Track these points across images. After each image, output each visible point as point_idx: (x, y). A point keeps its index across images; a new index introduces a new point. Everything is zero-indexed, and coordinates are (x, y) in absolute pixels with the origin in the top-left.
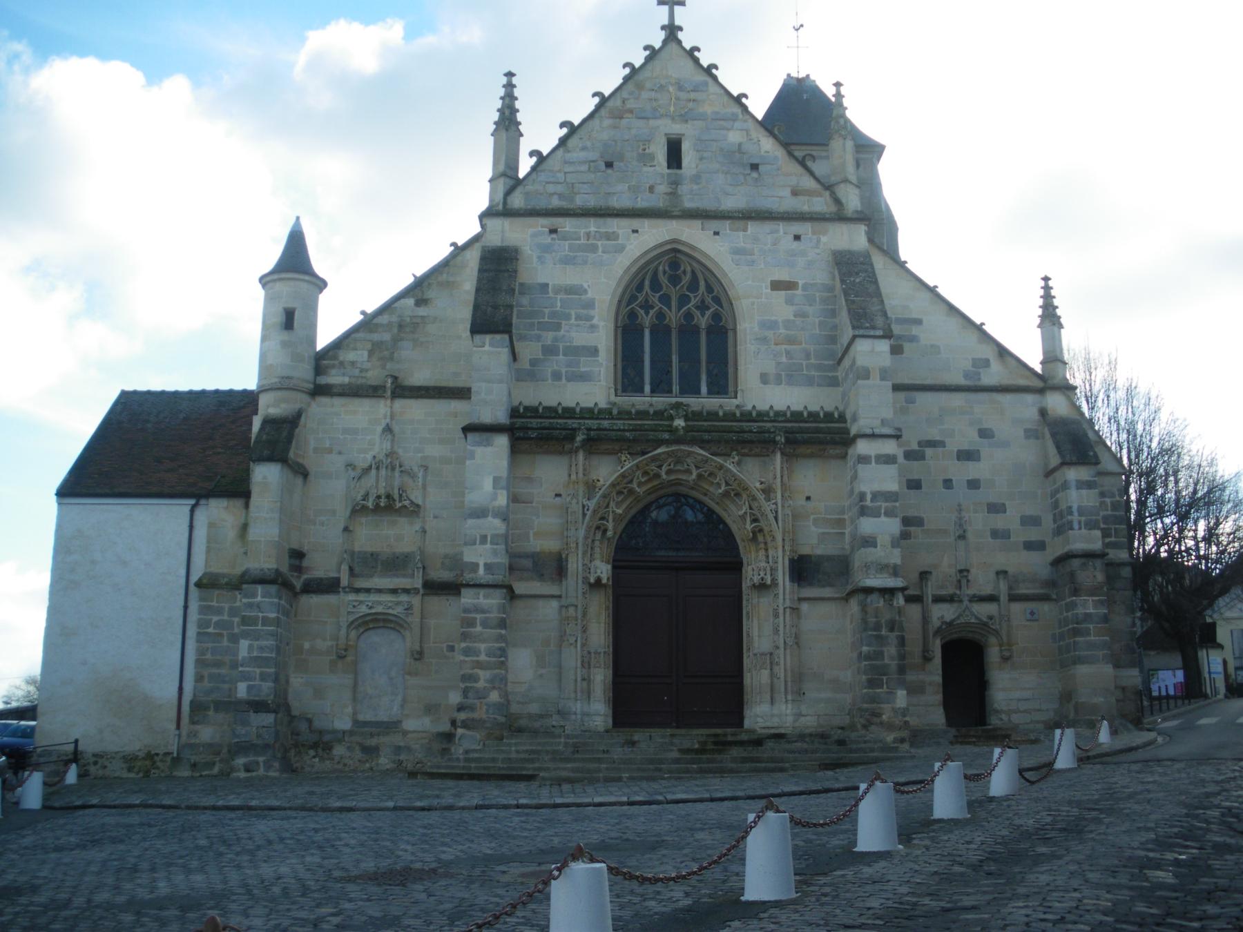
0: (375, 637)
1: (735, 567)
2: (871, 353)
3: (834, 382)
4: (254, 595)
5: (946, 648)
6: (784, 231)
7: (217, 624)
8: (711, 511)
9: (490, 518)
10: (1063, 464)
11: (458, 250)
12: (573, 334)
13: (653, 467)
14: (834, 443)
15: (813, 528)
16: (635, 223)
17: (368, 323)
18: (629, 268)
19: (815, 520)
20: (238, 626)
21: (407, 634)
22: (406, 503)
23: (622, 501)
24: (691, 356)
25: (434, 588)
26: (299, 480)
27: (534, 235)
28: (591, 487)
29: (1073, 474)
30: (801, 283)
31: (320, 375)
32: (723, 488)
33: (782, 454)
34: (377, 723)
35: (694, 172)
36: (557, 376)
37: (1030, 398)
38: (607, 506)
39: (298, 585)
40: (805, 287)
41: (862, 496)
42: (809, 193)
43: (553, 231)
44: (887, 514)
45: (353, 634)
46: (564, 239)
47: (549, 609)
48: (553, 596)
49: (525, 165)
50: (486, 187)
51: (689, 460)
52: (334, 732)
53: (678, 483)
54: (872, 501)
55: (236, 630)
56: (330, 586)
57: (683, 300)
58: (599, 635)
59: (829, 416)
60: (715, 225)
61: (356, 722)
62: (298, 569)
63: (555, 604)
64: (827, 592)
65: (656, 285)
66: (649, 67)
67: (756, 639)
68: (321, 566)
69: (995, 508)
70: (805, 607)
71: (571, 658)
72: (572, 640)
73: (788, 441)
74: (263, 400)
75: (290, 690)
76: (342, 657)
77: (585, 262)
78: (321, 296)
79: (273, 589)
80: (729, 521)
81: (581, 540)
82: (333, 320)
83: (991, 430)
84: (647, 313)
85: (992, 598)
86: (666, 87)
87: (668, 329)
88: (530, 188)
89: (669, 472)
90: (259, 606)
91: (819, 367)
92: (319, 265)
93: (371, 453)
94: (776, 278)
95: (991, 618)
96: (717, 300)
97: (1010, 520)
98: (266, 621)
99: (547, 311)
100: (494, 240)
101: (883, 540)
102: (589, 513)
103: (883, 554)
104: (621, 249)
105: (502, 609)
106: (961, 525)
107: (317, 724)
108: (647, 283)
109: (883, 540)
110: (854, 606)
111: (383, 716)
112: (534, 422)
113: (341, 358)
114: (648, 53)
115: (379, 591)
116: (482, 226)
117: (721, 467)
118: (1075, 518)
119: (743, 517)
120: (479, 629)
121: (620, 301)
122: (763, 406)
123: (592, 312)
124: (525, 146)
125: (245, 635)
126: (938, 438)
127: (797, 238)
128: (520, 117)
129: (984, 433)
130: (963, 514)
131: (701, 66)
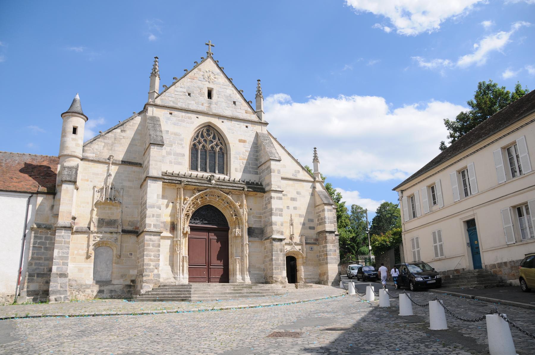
3: (257, 173)
4: (61, 233)
6: (243, 125)
7: (39, 243)
24: (204, 160)
36: (171, 162)
43: (171, 114)
52: (86, 285)
55: (48, 246)
59: (257, 184)
65: (202, 136)
91: (253, 168)
102: (185, 209)
104: (193, 123)
107: (79, 282)
120: (151, 247)
129: (298, 193)
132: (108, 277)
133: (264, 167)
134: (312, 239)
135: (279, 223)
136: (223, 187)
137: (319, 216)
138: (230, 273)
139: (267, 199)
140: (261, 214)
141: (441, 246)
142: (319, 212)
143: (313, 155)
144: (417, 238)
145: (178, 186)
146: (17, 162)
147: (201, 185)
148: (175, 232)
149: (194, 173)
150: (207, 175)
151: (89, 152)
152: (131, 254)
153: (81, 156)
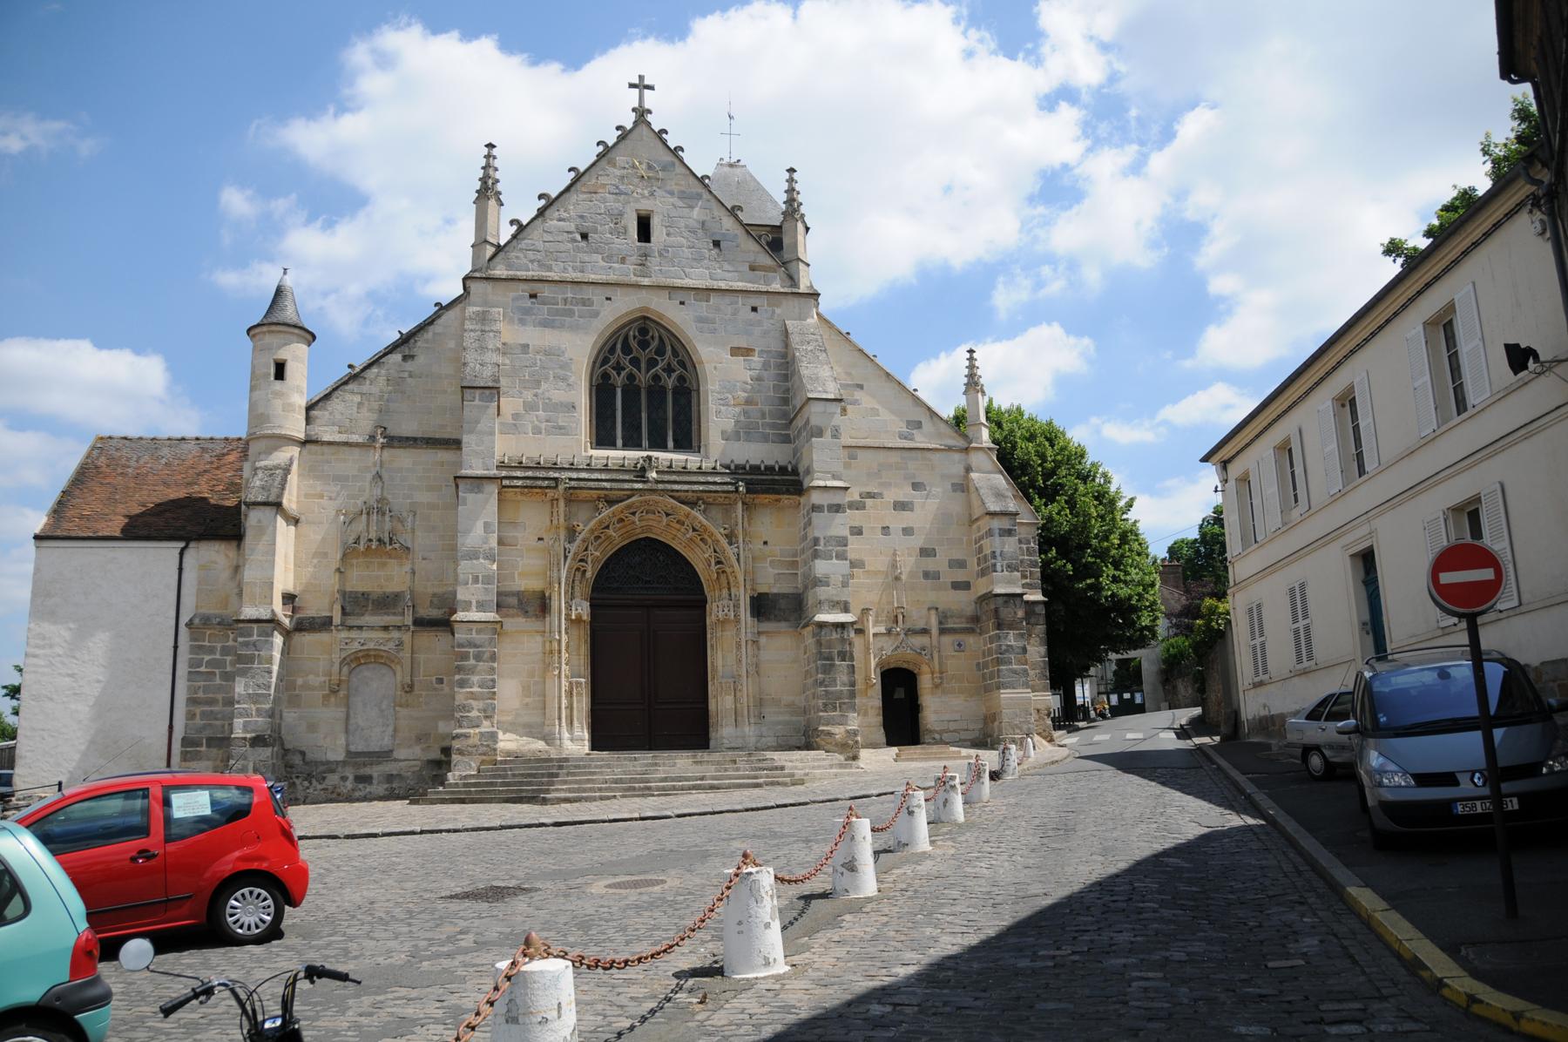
3: (786, 440)
7: (209, 663)
36: (537, 431)
43: (533, 296)
52: (328, 762)
55: (229, 669)
59: (783, 470)
65: (627, 349)
85: (925, 631)
91: (773, 426)
107: (309, 756)
120: (472, 662)
133: (799, 422)
134: (960, 617)
135: (836, 579)
136: (676, 487)
140: (795, 555)
141: (1307, 629)
142: (981, 538)
143: (966, 372)
144: (1259, 606)
145: (551, 493)
146: (163, 461)
147: (615, 485)
150: (634, 455)
152: (440, 681)
153: (302, 436)
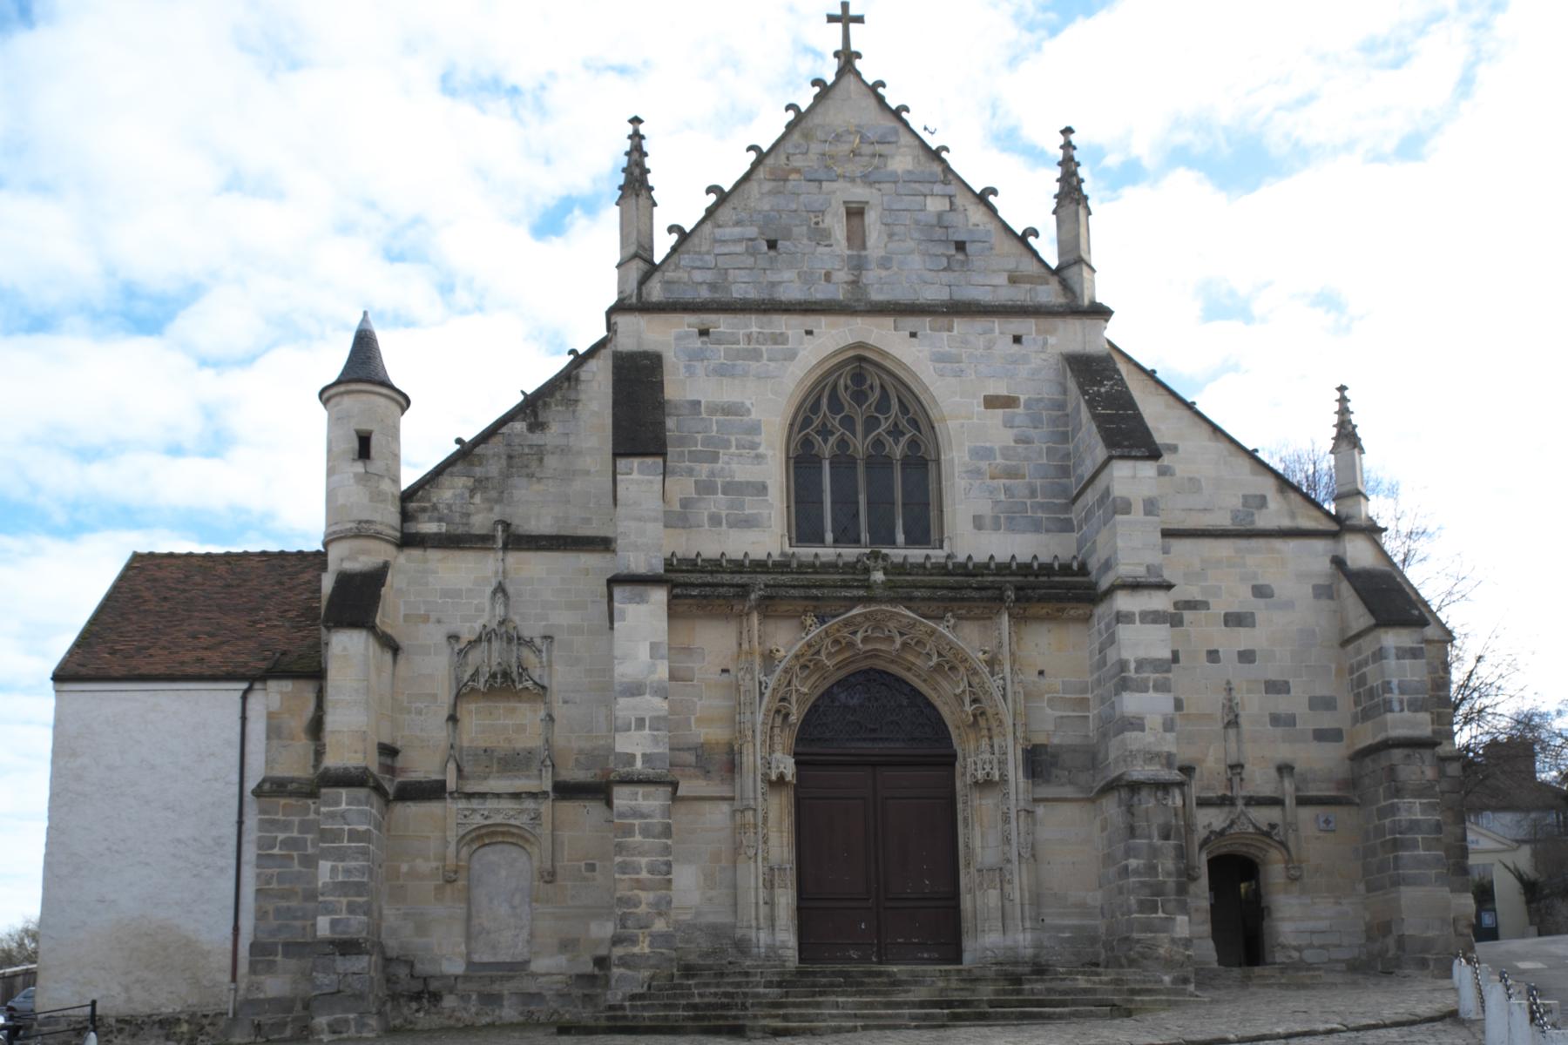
0: (492, 855)
1: (948, 760)
2: (1130, 478)
3: (1066, 527)
4: (338, 803)
5: (1214, 863)
6: (1001, 329)
7: (284, 843)
8: (915, 692)
9: (647, 697)
10: (1377, 625)
11: (579, 360)
12: (734, 466)
13: (845, 632)
14: (1078, 599)
15: (1048, 711)
16: (810, 321)
17: (466, 453)
18: (802, 381)
19: (1050, 700)
20: (314, 845)
21: (535, 851)
22: (529, 684)
23: (807, 678)
24: (845, 502)
25: (566, 791)
26: (388, 657)
27: (679, 338)
28: (769, 658)
29: (1392, 639)
30: (1022, 398)
31: (418, 519)
32: (935, 659)
33: (1010, 615)
34: (498, 964)
35: (882, 253)
36: (715, 520)
37: (1320, 545)
38: (789, 684)
39: (390, 789)
40: (1028, 405)
41: (1123, 665)
42: (1030, 279)
43: (704, 333)
44: (1157, 688)
45: (465, 852)
46: (719, 342)
47: (718, 815)
48: (723, 799)
49: (662, 245)
50: (614, 275)
51: (891, 625)
52: (443, 977)
53: (875, 654)
54: (1137, 670)
55: (310, 851)
56: (432, 791)
57: (872, 423)
58: (780, 846)
59: (1066, 569)
60: (911, 323)
61: (470, 964)
62: (391, 770)
63: (725, 807)
64: (1068, 792)
66: (819, 110)
67: (978, 850)
68: (422, 766)
69: (1276, 687)
70: (1040, 810)
71: (751, 876)
72: (751, 852)
73: (1018, 600)
74: (334, 554)
75: (384, 925)
76: (450, 881)
77: (745, 374)
78: (403, 419)
79: (362, 793)
80: (938, 703)
81: (759, 728)
82: (421, 447)
83: (1268, 586)
84: (826, 441)
85: (1276, 802)
86: (845, 137)
87: (852, 461)
88: (670, 275)
89: (865, 640)
90: (343, 815)
92: (397, 375)
93: (481, 622)
94: (991, 392)
95: (1273, 826)
96: (914, 423)
97: (1294, 704)
98: (354, 836)
99: (699, 437)
100: (625, 343)
101: (1154, 721)
102: (768, 693)
103: (1152, 739)
105: (668, 812)
106: (1231, 708)
108: (825, 401)
109: (1154, 721)
110: (1111, 807)
111: (504, 957)
112: (694, 578)
113: (434, 500)
114: (817, 90)
115: (498, 796)
116: (610, 326)
117: (933, 632)
118: (1395, 696)
119: (959, 698)
120: (638, 838)
121: (791, 425)
122: (980, 557)
123: (757, 439)
124: (662, 219)
125: (325, 854)
126: (1199, 598)
127: (1017, 339)
128: (652, 179)
129: (1261, 592)
130: (1234, 693)
131: (889, 108)
132: (519, 952)
137: (1362, 680)
138: (964, 930)
139: (1102, 625)
140: (1085, 690)
142: (1360, 665)
148: (737, 781)
149: (806, 552)
151: (426, 516)
